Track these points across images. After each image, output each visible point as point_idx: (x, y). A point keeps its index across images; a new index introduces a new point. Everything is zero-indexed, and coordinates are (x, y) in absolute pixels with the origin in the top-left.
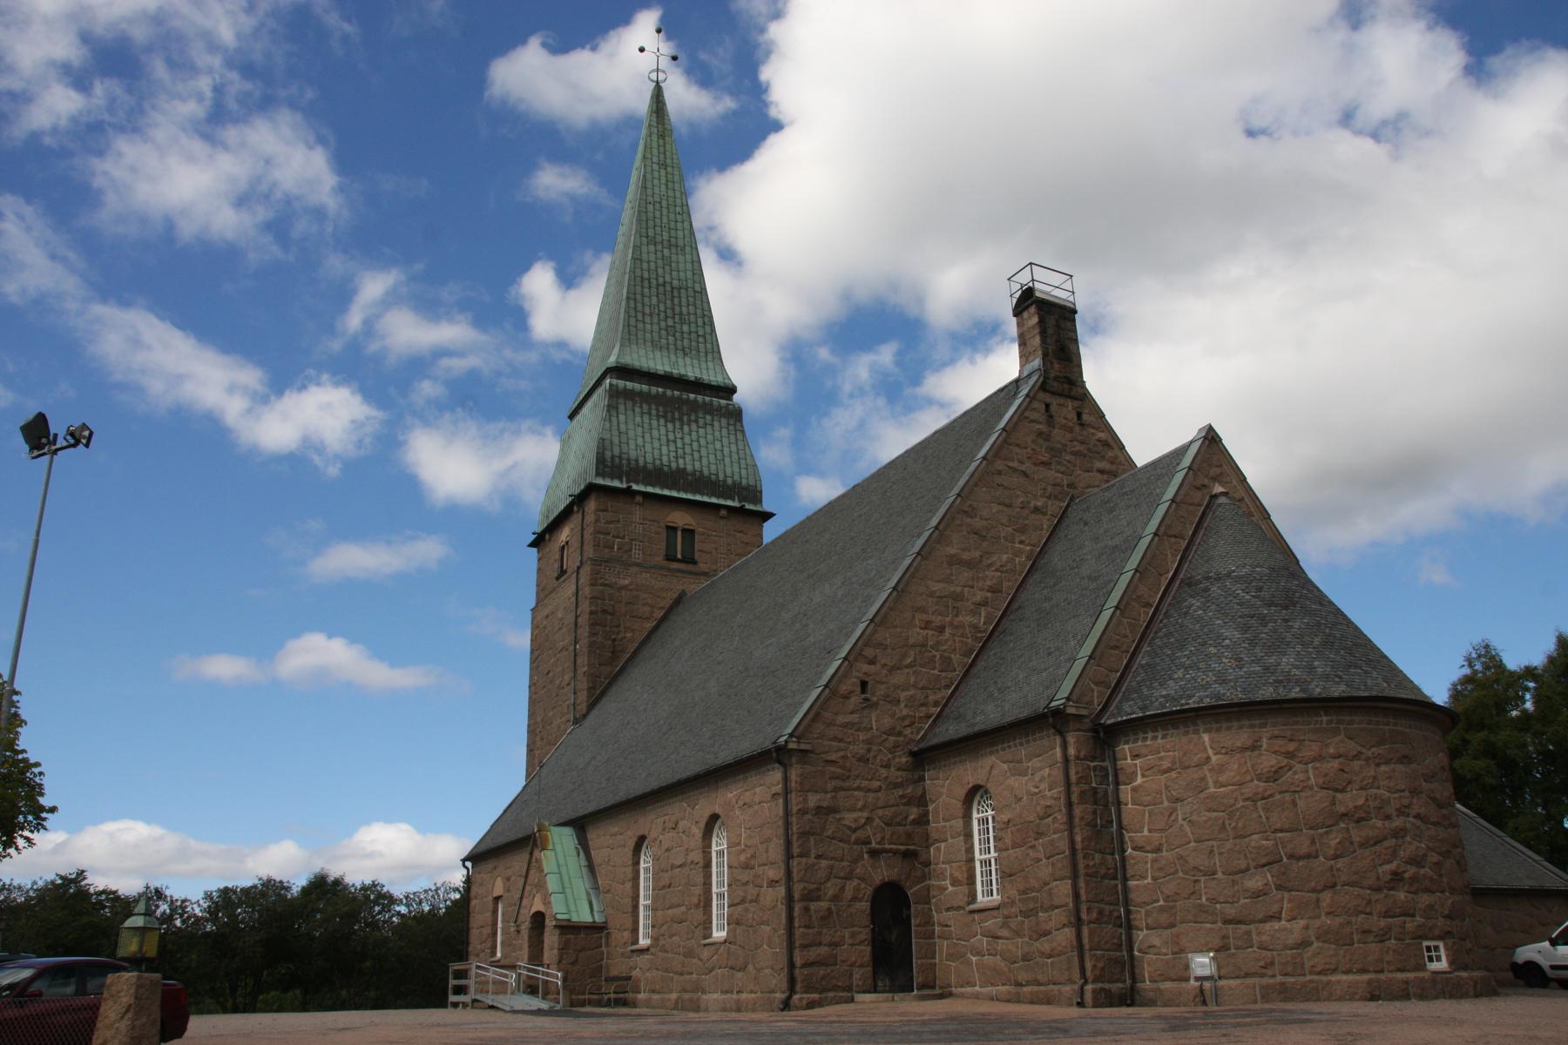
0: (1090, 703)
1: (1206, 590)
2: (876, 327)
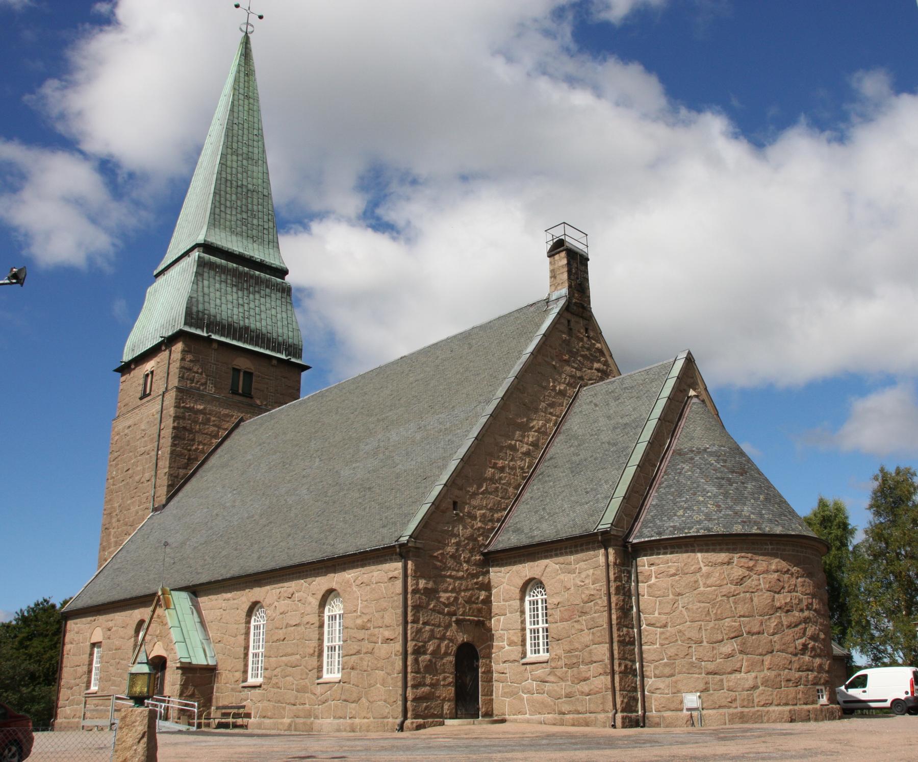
1: (692, 459)
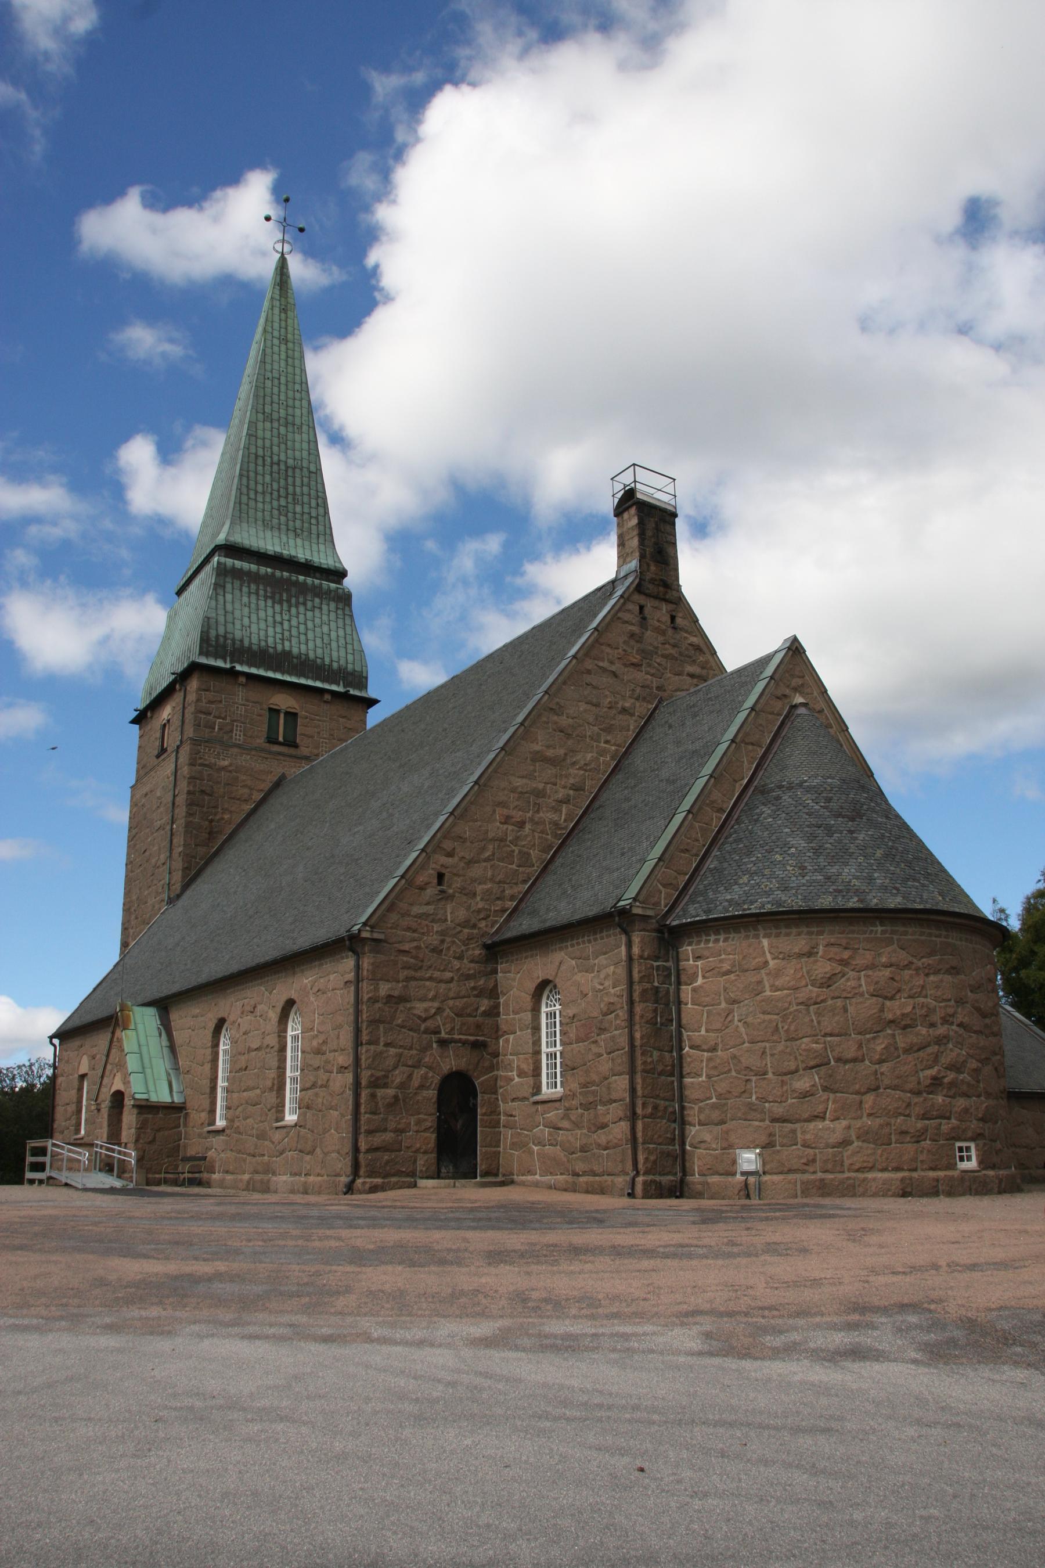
0: (657, 904)
1: (778, 798)
2: (480, 515)
